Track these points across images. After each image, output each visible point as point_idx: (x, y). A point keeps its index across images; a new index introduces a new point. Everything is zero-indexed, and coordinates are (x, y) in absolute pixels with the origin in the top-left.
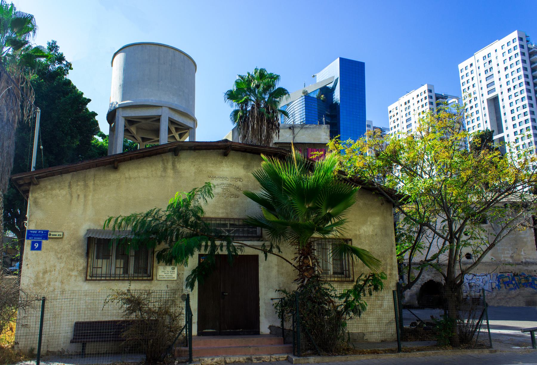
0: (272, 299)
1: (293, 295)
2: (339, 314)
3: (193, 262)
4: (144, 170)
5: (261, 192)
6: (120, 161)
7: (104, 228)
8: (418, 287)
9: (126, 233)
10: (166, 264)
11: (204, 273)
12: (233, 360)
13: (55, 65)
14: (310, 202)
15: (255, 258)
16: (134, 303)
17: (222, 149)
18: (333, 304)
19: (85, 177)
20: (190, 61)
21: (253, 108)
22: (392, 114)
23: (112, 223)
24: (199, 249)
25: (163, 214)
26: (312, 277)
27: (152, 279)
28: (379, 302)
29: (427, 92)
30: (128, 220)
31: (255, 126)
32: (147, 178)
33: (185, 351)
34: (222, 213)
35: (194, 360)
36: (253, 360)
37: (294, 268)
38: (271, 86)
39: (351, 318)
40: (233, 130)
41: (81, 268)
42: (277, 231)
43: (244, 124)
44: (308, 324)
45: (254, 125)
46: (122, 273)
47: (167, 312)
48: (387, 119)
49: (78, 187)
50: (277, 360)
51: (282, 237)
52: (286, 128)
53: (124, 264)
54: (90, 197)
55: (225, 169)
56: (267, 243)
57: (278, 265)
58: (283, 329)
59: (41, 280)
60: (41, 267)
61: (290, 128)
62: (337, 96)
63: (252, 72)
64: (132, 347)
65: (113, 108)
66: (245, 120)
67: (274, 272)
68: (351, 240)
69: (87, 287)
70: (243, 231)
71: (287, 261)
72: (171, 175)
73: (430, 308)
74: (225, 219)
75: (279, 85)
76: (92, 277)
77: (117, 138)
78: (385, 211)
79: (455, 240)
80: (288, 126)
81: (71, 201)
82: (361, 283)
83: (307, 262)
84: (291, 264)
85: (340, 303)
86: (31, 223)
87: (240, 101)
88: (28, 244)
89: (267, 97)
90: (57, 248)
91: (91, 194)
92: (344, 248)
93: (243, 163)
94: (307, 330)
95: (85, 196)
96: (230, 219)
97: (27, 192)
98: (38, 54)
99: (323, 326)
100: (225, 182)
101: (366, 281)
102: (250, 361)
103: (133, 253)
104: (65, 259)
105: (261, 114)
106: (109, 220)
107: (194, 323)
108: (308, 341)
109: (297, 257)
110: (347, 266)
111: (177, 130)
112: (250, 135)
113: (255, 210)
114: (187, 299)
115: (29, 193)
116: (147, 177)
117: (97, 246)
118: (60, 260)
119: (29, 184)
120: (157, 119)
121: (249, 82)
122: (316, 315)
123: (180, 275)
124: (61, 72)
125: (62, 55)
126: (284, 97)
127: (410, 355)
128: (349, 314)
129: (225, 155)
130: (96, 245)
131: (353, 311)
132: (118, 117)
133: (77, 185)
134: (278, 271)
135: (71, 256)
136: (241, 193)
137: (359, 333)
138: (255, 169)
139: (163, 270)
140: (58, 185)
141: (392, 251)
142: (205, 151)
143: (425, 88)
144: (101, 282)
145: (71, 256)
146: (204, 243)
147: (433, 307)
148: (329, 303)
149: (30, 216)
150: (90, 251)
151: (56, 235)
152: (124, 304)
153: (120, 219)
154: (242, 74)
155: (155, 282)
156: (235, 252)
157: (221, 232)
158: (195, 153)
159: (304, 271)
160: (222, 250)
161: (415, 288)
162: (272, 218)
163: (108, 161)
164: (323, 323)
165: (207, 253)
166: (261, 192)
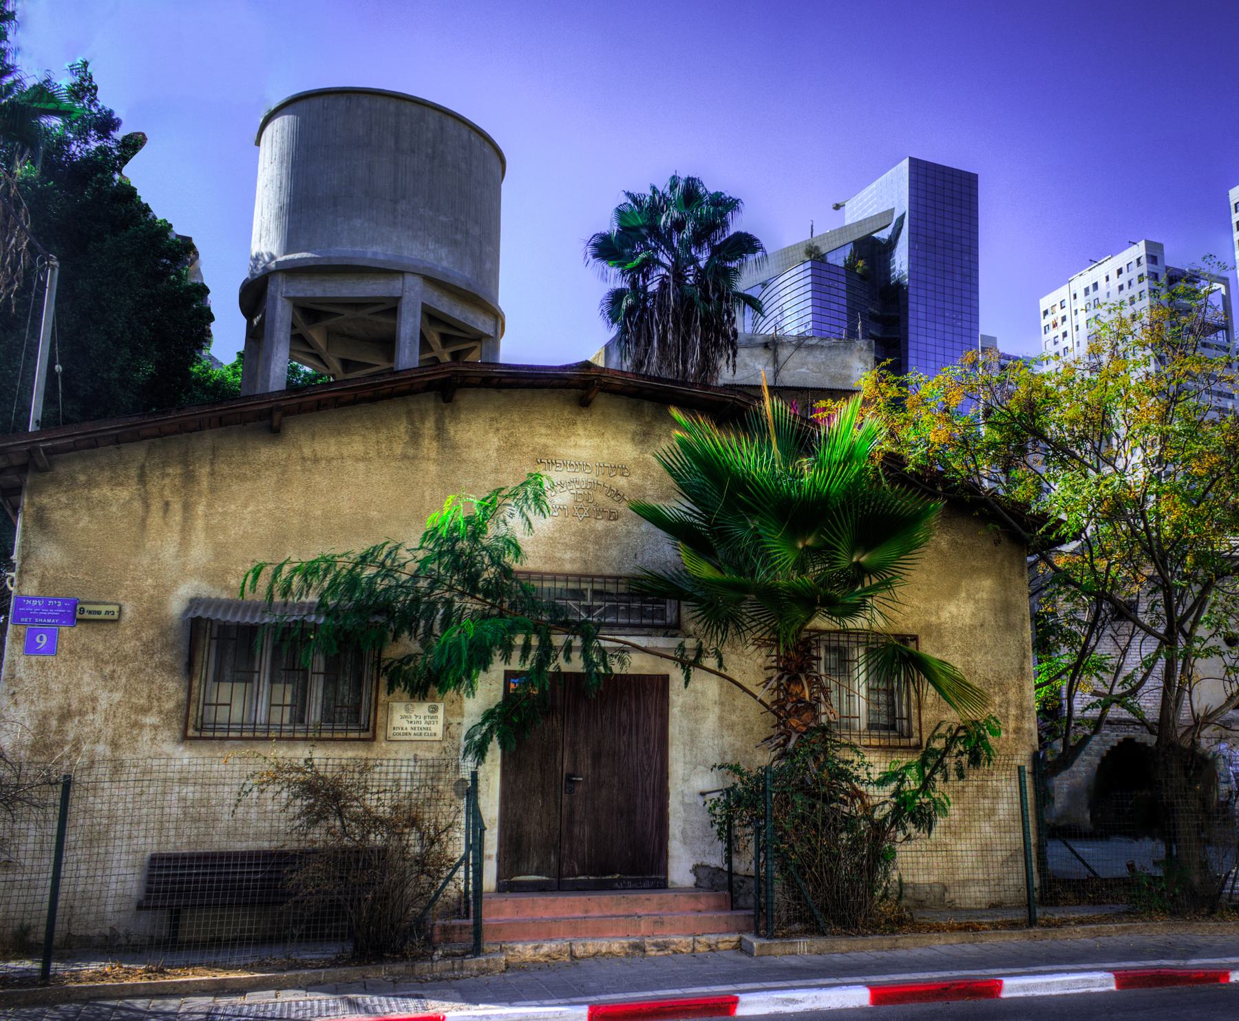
0: (703, 794)
1: (758, 778)
2: (879, 830)
3: (488, 689)
4: (356, 438)
5: (677, 506)
6: (289, 412)
7: (242, 594)
8: (1090, 764)
9: (301, 609)
10: (412, 697)
11: (516, 720)
12: (591, 949)
13: (87, 143)
14: (810, 535)
15: (661, 684)
16: (324, 796)
17: (576, 389)
18: (863, 802)
19: (186, 453)
20: (487, 149)
21: (663, 285)
22: (1049, 320)
23: (263, 582)
24: (507, 658)
25: (409, 556)
26: (810, 730)
27: (374, 738)
28: (987, 803)
29: (1143, 260)
30: (309, 571)
31: (670, 337)
32: (363, 459)
33: (462, 927)
34: (573, 561)
35: (486, 948)
36: (648, 948)
37: (764, 709)
38: (717, 226)
39: (908, 838)
40: (607, 348)
41: (170, 705)
42: (721, 610)
43: (640, 329)
44: (794, 852)
45: (665, 332)
46: (286, 719)
47: (414, 822)
48: (1035, 330)
49: (167, 481)
50: (712, 948)
51: (731, 626)
52: (756, 346)
53: (294, 696)
54: (201, 509)
55: (583, 442)
56: (690, 643)
57: (722, 704)
58: (730, 873)
59: (53, 737)
60: (55, 702)
61: (766, 346)
62: (901, 262)
63: (663, 186)
64: (316, 914)
65: (259, 272)
66: (641, 318)
67: (710, 722)
68: (915, 638)
69: (185, 757)
70: (629, 612)
71: (745, 690)
72: (433, 455)
73: (1125, 834)
74: (580, 577)
75: (738, 224)
76: (201, 729)
77: (268, 359)
78: (1006, 564)
79: (1181, 637)
80: (760, 339)
81: (144, 520)
82: (939, 745)
83: (797, 689)
84: (755, 697)
85: (880, 796)
86: (25, 577)
87: (629, 266)
88: (17, 636)
89: (703, 258)
90: (100, 648)
91: (204, 501)
92: (900, 659)
93: (632, 427)
94: (792, 868)
95: (187, 507)
96: (593, 577)
97: (17, 490)
98: (42, 106)
99: (836, 858)
100: (582, 476)
101: (953, 740)
102: (638, 953)
103: (319, 663)
104: (124, 680)
105: (686, 303)
106: (257, 573)
107: (490, 857)
108: (794, 898)
109: (770, 679)
110: (904, 708)
111: (446, 340)
112: (654, 359)
113: (664, 553)
114: (471, 792)
115: (20, 494)
116: (365, 459)
117: (219, 644)
118: (111, 684)
119: (24, 468)
120: (391, 308)
121: (655, 209)
122: (817, 830)
123: (452, 729)
124: (107, 162)
125: (111, 113)
126: (751, 258)
127: (1059, 934)
128: (904, 828)
129: (584, 403)
130: (214, 642)
131: (913, 820)
132: (274, 299)
133: (164, 475)
134: (721, 718)
135: (140, 670)
136: (622, 508)
137: (930, 885)
138: (664, 444)
139: (404, 713)
140: (107, 474)
141: (1022, 669)
142: (527, 392)
143: (1140, 250)
144: (228, 744)
145: (140, 670)
146: (519, 640)
147: (1133, 832)
148: (853, 798)
149: (24, 558)
150: (198, 659)
151: (99, 613)
152: (296, 796)
153: (286, 568)
154: (636, 191)
155: (380, 747)
156: (605, 666)
157: (568, 610)
158: (498, 397)
159: (789, 715)
160: (568, 659)
161: (1084, 768)
162: (705, 570)
163: (256, 415)
164: (835, 851)
165: (527, 667)
166: (677, 506)
